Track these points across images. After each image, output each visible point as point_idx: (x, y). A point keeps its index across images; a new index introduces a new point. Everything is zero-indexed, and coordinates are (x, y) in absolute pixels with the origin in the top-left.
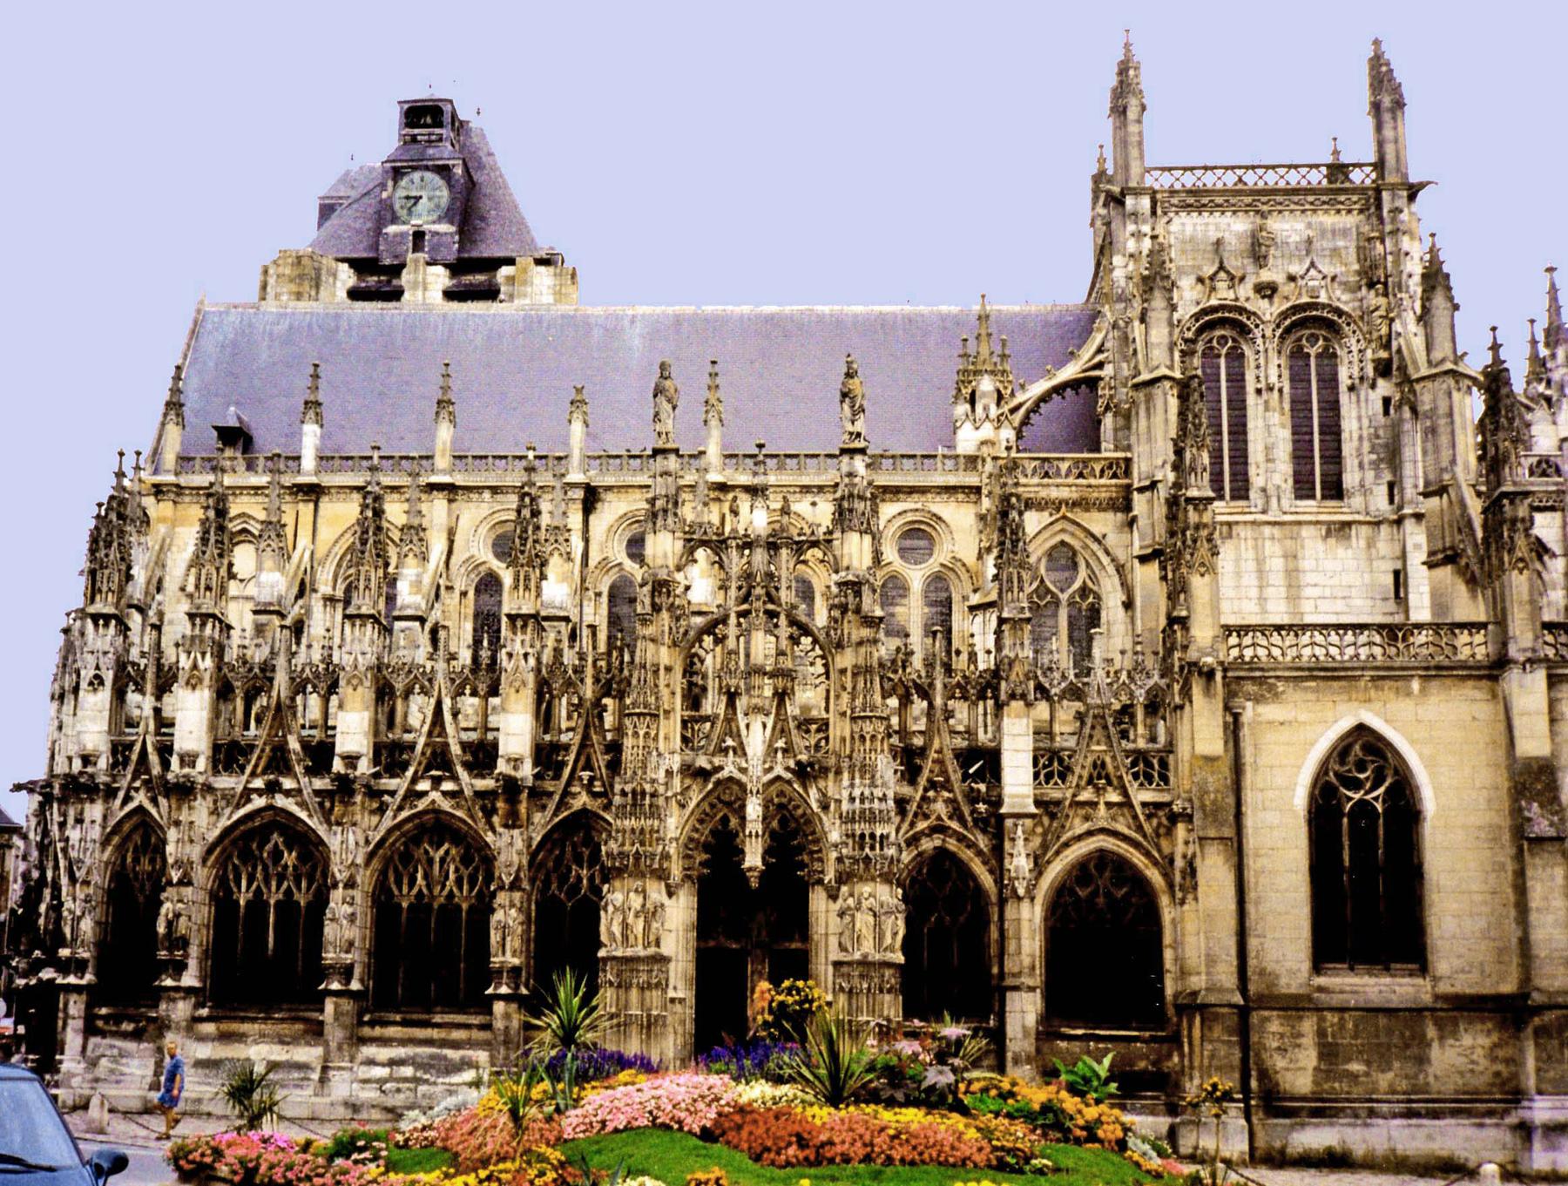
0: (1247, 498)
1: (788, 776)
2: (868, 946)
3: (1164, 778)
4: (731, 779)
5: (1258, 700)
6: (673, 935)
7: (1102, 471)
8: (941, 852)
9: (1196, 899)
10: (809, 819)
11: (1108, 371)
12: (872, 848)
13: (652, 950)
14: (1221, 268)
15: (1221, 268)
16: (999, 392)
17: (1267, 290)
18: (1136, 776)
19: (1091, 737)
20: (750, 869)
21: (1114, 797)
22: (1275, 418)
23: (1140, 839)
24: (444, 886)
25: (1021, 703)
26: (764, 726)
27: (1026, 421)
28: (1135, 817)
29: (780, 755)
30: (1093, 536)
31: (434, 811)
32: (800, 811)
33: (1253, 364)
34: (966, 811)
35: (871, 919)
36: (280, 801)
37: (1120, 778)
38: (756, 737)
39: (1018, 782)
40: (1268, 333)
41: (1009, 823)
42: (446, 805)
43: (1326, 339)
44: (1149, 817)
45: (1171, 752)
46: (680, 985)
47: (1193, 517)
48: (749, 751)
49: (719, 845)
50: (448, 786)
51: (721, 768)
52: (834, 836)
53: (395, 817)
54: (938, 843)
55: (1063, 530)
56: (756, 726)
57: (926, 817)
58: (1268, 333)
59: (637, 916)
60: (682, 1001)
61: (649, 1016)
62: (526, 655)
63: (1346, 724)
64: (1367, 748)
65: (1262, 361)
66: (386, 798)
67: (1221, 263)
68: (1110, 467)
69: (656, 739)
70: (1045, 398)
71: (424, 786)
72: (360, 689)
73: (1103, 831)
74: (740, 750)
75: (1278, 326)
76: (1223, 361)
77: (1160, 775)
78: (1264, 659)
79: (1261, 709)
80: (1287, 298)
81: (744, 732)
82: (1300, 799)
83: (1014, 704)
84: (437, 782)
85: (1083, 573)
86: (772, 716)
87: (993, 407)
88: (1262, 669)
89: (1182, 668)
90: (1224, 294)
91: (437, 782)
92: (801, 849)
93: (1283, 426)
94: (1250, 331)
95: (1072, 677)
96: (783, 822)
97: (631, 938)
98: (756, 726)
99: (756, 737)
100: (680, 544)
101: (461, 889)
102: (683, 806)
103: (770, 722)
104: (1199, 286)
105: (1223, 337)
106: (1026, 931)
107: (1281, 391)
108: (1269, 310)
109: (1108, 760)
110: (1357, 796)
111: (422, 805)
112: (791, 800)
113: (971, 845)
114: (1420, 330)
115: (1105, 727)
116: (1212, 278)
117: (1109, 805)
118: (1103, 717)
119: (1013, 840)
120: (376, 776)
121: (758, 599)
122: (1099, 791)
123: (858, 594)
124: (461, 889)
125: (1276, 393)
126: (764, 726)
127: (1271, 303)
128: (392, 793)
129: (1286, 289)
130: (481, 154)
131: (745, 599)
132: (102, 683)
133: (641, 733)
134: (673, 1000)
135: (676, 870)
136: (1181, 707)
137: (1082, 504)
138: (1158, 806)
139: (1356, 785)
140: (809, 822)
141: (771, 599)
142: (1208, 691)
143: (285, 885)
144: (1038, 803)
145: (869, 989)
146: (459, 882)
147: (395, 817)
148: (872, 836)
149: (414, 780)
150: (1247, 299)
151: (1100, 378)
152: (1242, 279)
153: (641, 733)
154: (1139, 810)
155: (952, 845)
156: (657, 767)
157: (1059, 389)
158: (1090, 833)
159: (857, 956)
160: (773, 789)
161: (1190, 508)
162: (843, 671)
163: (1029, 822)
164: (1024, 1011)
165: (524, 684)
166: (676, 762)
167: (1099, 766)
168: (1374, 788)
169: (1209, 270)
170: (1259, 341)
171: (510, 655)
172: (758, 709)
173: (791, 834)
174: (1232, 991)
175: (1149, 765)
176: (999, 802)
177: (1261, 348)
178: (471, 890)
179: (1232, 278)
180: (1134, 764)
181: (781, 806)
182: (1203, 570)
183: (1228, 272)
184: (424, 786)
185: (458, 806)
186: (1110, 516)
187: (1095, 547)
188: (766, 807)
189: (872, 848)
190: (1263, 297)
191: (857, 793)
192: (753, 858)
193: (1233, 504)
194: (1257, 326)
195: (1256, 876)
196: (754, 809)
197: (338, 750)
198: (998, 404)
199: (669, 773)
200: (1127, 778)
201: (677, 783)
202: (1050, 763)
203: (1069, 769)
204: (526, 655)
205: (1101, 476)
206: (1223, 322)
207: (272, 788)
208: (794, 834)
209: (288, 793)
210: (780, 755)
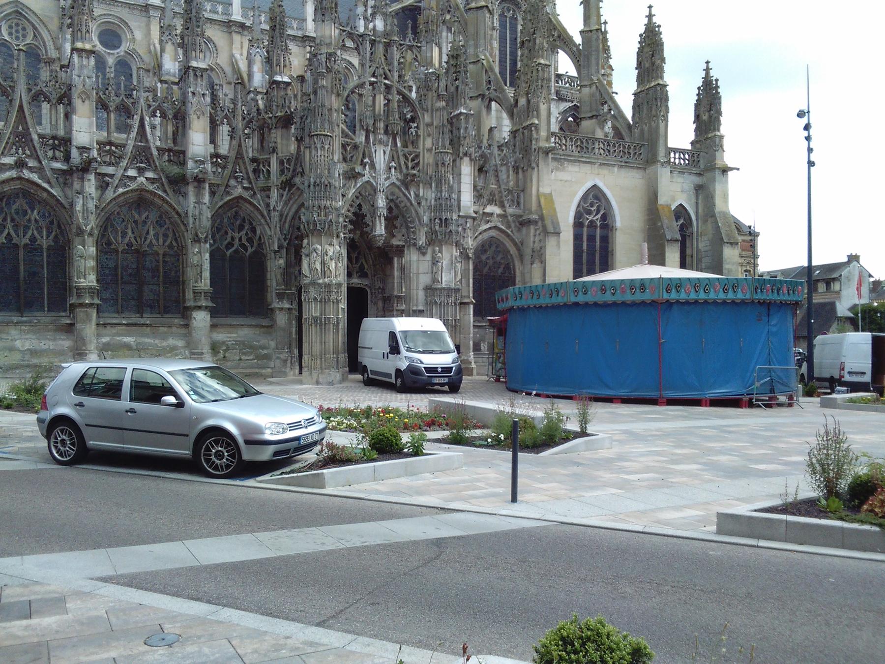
1: (398, 183)
4: (368, 182)
24: (146, 239)
29: (393, 170)
32: (403, 205)
36: (26, 174)
43: (514, 11)
49: (359, 220)
52: (426, 219)
53: (115, 192)
63: (589, 185)
64: (596, 197)
71: (132, 173)
72: (87, 102)
73: (496, 228)
74: (373, 166)
82: (571, 219)
91: (141, 171)
97: (328, 273)
101: (158, 240)
109: (496, 192)
110: (590, 218)
111: (133, 186)
112: (398, 198)
114: (234, 52)
124: (158, 240)
126: (384, 153)
128: (112, 176)
139: (589, 213)
143: (30, 233)
146: (156, 236)
147: (115, 192)
168: (597, 214)
171: (194, 93)
173: (396, 216)
178: (164, 241)
197: (74, 143)
209: (31, 169)
210: (393, 170)
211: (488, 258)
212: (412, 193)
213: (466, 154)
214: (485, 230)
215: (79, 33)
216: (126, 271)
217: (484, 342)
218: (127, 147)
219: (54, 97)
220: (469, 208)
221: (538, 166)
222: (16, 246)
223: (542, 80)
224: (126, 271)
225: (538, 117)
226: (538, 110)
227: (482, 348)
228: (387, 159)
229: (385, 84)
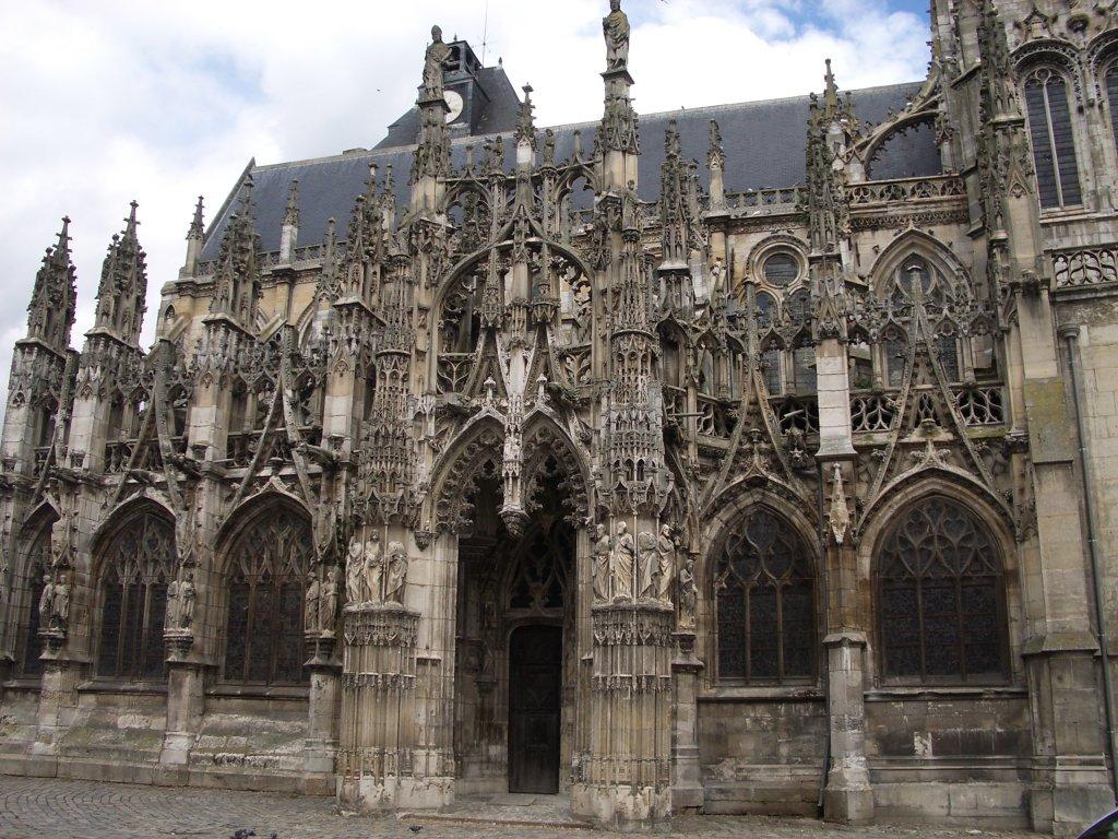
0: (1080, 202)
2: (623, 590)
3: (997, 413)
4: (488, 419)
5: (1093, 323)
6: (427, 590)
7: (944, 189)
8: (762, 508)
9: (1037, 534)
10: (573, 457)
11: (942, 107)
12: (629, 478)
13: (392, 604)
14: (1035, 12)
15: (1035, 12)
16: (846, 134)
17: (1078, 24)
18: (966, 413)
19: (915, 375)
20: (507, 514)
21: (944, 435)
22: (1098, 129)
23: (979, 483)
25: (835, 342)
26: (526, 361)
27: (872, 157)
28: (967, 455)
30: (939, 244)
31: (273, 494)
33: (1073, 89)
34: (784, 460)
35: (627, 559)
37: (949, 415)
38: (517, 375)
39: (835, 426)
40: (1084, 58)
41: (826, 466)
42: (282, 488)
43: (1053, 71)
44: (983, 454)
45: (1002, 384)
46: (437, 645)
47: (1001, 140)
48: (509, 389)
50: (287, 471)
51: (478, 408)
54: (757, 497)
55: (912, 245)
56: (517, 362)
57: (743, 470)
58: (1084, 58)
59: (371, 567)
60: (435, 662)
61: (384, 677)
62: (350, 341)
65: (1080, 85)
66: (236, 485)
67: (1035, 9)
68: (950, 185)
69: (406, 378)
70: (886, 137)
71: (266, 472)
73: (933, 472)
74: (500, 390)
75: (1093, 53)
76: (1045, 89)
77: (992, 410)
78: (1095, 280)
79: (1097, 331)
80: (1098, 29)
81: (505, 369)
83: (826, 343)
84: (278, 466)
85: (934, 280)
86: (533, 351)
87: (842, 147)
88: (1096, 291)
89: (1004, 291)
90: (1039, 32)
92: (568, 493)
93: (1107, 137)
94: (1067, 61)
95: (890, 316)
96: (551, 465)
98: (517, 362)
99: (517, 375)
100: (441, 188)
102: (435, 452)
103: (531, 355)
104: (1017, 31)
105: (1042, 71)
106: (850, 580)
107: (1100, 107)
108: (1082, 40)
109: (935, 398)
112: (554, 438)
113: (791, 497)
115: (930, 364)
116: (1026, 22)
117: (938, 445)
118: (927, 354)
119: (831, 484)
120: (228, 465)
121: (520, 232)
122: (928, 430)
123: (619, 210)
125: (1096, 108)
126: (526, 361)
127: (1084, 36)
128: (239, 480)
129: (1095, 20)
130: (499, 84)
131: (509, 236)
132: (23, 401)
133: (388, 373)
134: (423, 662)
135: (428, 522)
136: (1008, 331)
137: (927, 219)
138: (990, 441)
140: (572, 461)
141: (533, 232)
142: (1034, 312)
144: (855, 447)
145: (623, 641)
147: (728, 481)
148: (629, 463)
149: (258, 468)
150: (1062, 35)
151: (937, 115)
152: (1055, 19)
153: (388, 373)
154: (969, 445)
155: (774, 499)
156: (406, 410)
157: (899, 128)
158: (919, 476)
159: (610, 603)
160: (536, 430)
161: (999, 133)
162: (604, 293)
163: (847, 466)
164: (848, 670)
165: (347, 367)
166: (428, 404)
167: (925, 404)
169: (1023, 17)
170: (1077, 68)
172: (519, 344)
173: (555, 476)
174: (1082, 635)
175: (980, 400)
176: (812, 450)
177: (1079, 73)
179: (1046, 19)
180: (963, 401)
181: (545, 447)
182: (1018, 191)
183: (1041, 16)
184: (266, 472)
185: (292, 489)
186: (954, 227)
187: (943, 255)
188: (526, 449)
189: (629, 478)
190: (1076, 31)
191: (614, 416)
192: (513, 502)
193: (1067, 208)
194: (1073, 55)
195: (1106, 509)
196: (512, 450)
198: (847, 145)
199: (419, 416)
200: (957, 416)
201: (431, 427)
202: (868, 407)
203: (893, 411)
204: (350, 341)
205: (943, 194)
206: (1041, 58)
207: (144, 482)
208: (560, 477)
211: (929, 541)
212: (572, 430)
213: (825, 335)
214: (907, 482)
215: (817, 235)
216: (260, 617)
217: (922, 730)
218: (742, 405)
219: (788, 341)
220: (841, 438)
221: (1017, 325)
222: (772, 589)
223: (1008, 152)
224: (260, 617)
225: (1006, 227)
226: (1002, 212)
227: (918, 746)
228: (529, 365)
229: (528, 245)
